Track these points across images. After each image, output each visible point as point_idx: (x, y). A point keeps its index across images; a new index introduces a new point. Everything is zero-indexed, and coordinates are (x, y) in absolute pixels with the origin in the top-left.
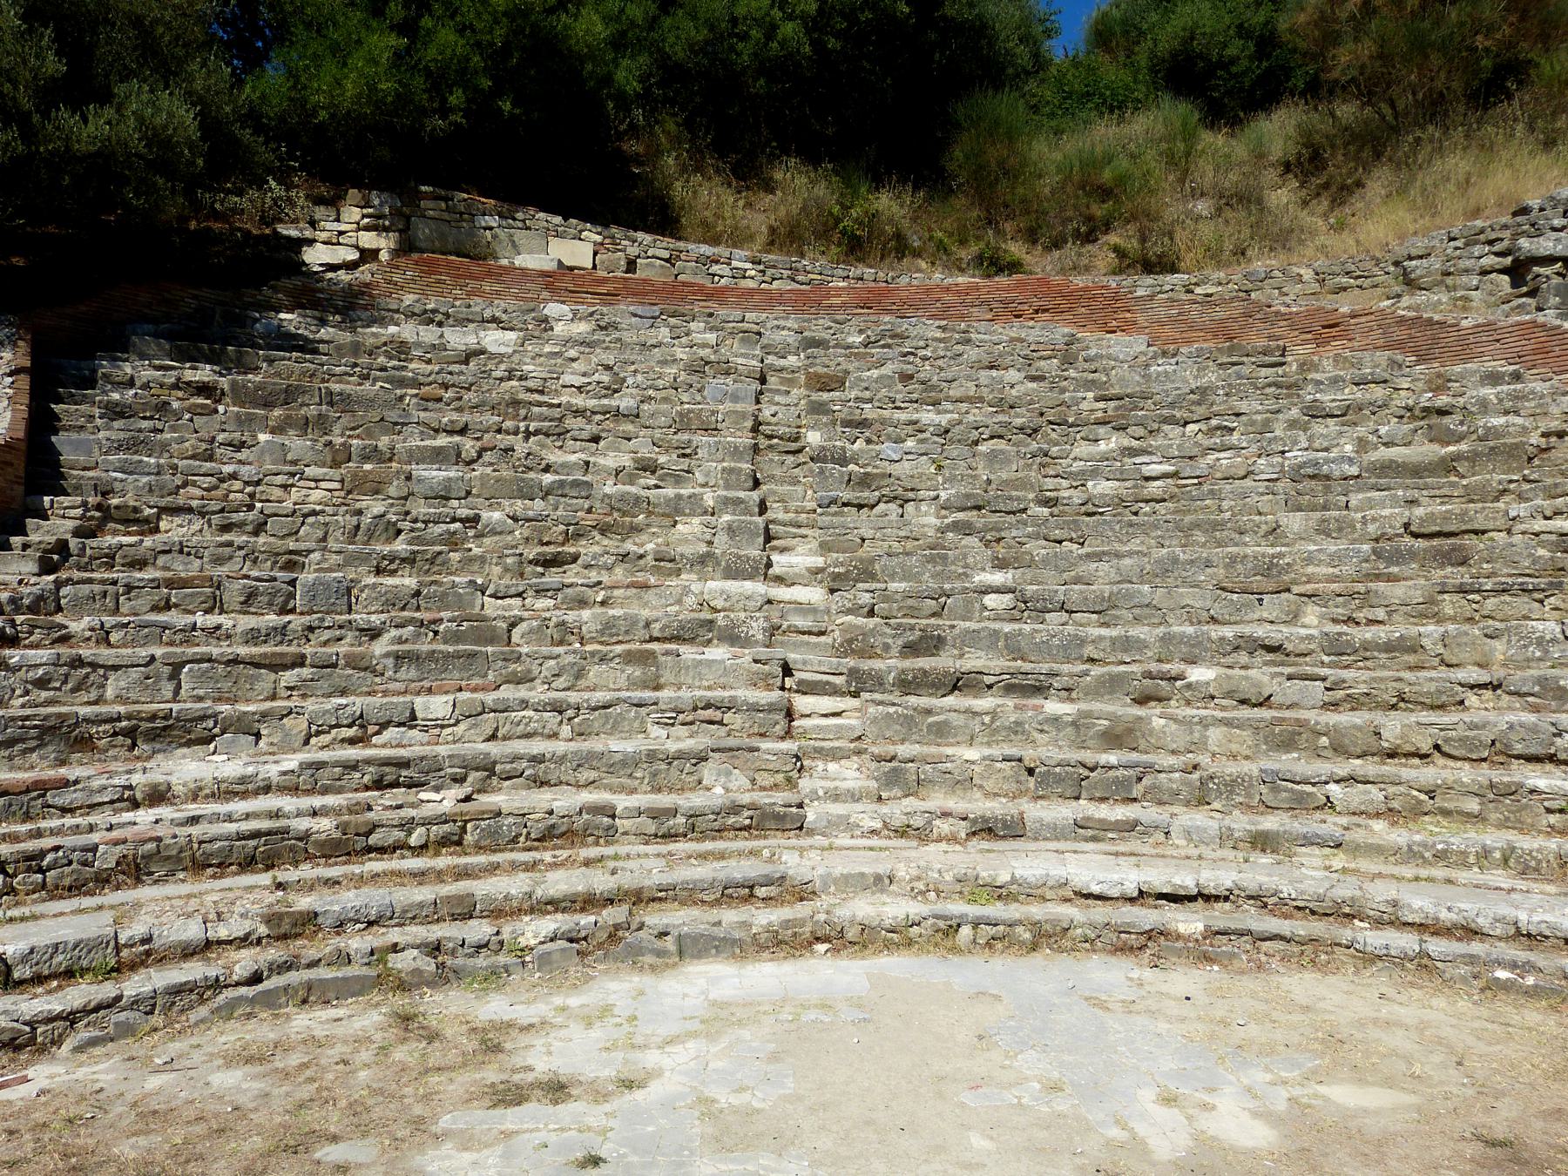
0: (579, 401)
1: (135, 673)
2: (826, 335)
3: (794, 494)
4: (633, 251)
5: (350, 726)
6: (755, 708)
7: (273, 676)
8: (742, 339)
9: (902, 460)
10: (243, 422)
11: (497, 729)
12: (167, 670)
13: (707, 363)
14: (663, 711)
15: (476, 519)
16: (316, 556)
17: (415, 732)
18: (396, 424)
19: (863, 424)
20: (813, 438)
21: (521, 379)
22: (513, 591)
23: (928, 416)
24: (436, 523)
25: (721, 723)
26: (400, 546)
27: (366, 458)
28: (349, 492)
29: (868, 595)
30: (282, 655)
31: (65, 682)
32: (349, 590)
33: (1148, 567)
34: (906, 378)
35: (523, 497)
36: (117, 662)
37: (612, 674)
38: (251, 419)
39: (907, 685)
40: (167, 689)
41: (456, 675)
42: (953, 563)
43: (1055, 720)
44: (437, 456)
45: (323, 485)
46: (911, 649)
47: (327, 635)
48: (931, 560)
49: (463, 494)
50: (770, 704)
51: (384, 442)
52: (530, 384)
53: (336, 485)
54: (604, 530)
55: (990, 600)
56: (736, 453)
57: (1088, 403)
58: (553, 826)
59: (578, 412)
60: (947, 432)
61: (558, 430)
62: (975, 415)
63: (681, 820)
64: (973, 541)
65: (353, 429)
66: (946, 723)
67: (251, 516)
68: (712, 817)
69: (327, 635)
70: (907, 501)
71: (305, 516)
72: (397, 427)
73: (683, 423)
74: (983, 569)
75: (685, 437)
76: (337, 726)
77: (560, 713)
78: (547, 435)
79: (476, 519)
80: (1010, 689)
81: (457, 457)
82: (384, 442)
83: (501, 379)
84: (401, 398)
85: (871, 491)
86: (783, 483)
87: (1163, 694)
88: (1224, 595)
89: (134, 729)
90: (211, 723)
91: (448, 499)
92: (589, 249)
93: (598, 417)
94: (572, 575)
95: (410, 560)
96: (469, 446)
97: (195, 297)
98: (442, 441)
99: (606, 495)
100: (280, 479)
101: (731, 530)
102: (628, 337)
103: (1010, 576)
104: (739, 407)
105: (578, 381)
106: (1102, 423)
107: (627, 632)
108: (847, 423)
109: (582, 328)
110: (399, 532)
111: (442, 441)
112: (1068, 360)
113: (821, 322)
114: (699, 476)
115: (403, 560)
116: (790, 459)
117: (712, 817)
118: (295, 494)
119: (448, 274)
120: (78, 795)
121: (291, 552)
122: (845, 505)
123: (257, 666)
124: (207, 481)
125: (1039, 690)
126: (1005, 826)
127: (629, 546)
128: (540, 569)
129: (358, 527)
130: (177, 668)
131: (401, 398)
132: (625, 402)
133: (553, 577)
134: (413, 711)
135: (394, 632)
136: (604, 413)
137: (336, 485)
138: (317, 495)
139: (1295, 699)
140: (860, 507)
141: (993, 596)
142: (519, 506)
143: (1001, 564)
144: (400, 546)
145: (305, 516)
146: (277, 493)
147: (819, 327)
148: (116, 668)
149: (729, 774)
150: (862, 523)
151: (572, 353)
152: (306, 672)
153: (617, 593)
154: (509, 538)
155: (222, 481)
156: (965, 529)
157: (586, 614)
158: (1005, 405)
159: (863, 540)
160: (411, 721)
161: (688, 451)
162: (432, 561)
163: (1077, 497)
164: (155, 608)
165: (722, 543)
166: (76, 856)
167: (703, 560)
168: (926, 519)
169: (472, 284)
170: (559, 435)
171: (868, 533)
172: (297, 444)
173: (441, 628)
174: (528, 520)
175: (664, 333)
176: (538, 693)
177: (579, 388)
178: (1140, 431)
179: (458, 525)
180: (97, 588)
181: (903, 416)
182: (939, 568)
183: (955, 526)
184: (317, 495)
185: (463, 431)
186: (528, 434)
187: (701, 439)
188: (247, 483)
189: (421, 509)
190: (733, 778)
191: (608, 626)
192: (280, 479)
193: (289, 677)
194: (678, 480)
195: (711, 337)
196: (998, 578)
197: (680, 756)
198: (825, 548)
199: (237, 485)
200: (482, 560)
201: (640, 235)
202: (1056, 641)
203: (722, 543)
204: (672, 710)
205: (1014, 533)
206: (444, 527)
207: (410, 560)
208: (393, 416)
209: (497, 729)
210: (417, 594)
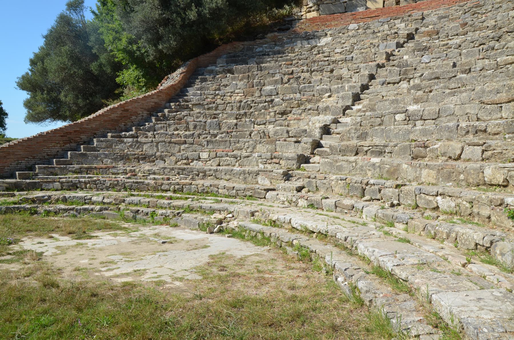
1: (149, 145)
5: (185, 159)
7: (179, 147)
8: (415, 23)
11: (220, 163)
12: (155, 144)
13: (388, 35)
14: (263, 159)
15: (272, 101)
16: (221, 115)
17: (200, 162)
18: (272, 74)
21: (322, 53)
22: (262, 123)
24: (261, 103)
25: (279, 163)
28: (246, 96)
29: (359, 118)
30: (180, 141)
31: (135, 146)
32: (219, 124)
33: (473, 96)
35: (293, 93)
36: (145, 142)
37: (263, 147)
40: (155, 149)
41: (222, 147)
42: (400, 103)
43: (374, 165)
45: (239, 95)
47: (204, 136)
49: (275, 94)
50: (292, 157)
52: (326, 54)
53: (242, 94)
58: (204, 189)
60: (460, 46)
61: (320, 69)
63: (234, 191)
65: (261, 77)
66: (341, 166)
67: (214, 105)
68: (242, 191)
69: (204, 136)
70: (411, 79)
71: (227, 104)
74: (410, 104)
76: (182, 159)
77: (237, 158)
78: (317, 71)
83: (316, 54)
84: (281, 65)
87: (422, 155)
88: (483, 106)
89: (138, 157)
90: (154, 157)
91: (272, 96)
93: (340, 63)
97: (243, 45)
99: (317, 90)
100: (229, 94)
103: (419, 106)
107: (281, 135)
110: (252, 107)
113: (454, 8)
115: (243, 115)
117: (242, 191)
118: (233, 98)
119: (319, 22)
120: (116, 170)
121: (215, 114)
122: (389, 83)
123: (175, 144)
124: (211, 97)
126: (317, 204)
128: (280, 116)
129: (240, 106)
130: (157, 143)
131: (281, 65)
134: (199, 156)
135: (220, 135)
136: (342, 61)
137: (242, 94)
139: (470, 157)
140: (394, 83)
141: (398, 115)
145: (227, 104)
146: (229, 98)
148: (145, 143)
149: (264, 179)
152: (186, 146)
153: (291, 122)
154: (281, 107)
155: (215, 96)
159: (383, 97)
160: (199, 159)
161: (358, 70)
162: (250, 115)
164: (174, 130)
166: (102, 182)
169: (328, 23)
170: (321, 70)
173: (232, 134)
174: (286, 100)
177: (340, 53)
179: (266, 103)
180: (162, 125)
182: (395, 105)
188: (221, 96)
190: (265, 181)
192: (229, 94)
193: (183, 147)
199: (219, 97)
202: (401, 132)
204: (265, 158)
205: (436, 87)
206: (262, 104)
209: (220, 163)
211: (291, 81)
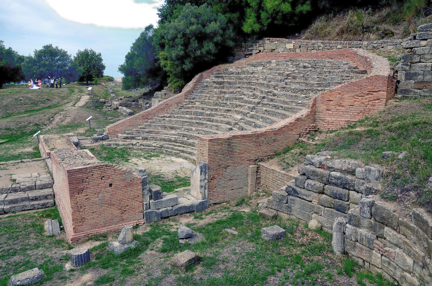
4: (300, 44)
92: (292, 45)
211: (237, 93)
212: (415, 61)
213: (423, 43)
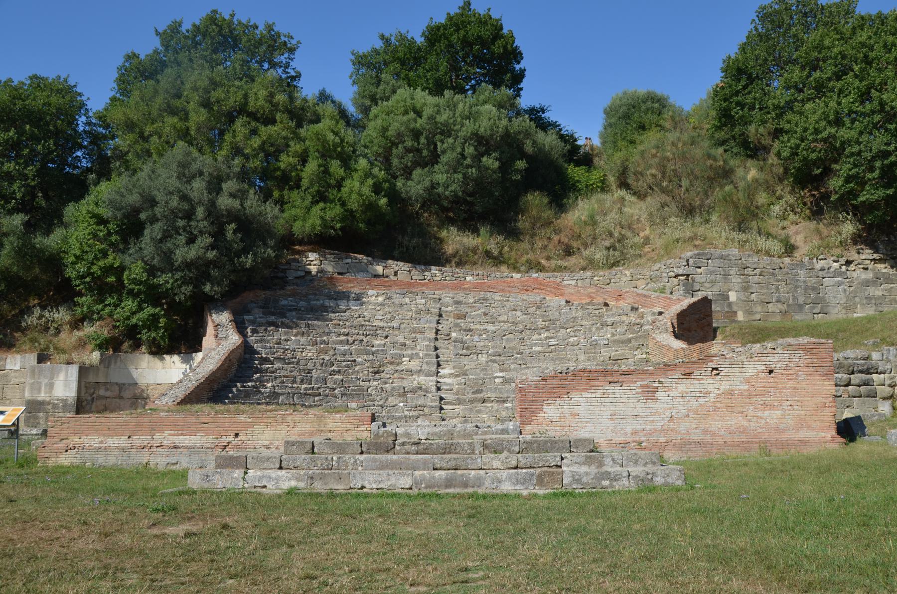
0: (381, 324)
2: (462, 299)
3: (447, 352)
4: (397, 268)
6: (432, 407)
9: (477, 341)
10: (286, 333)
19: (470, 330)
20: (454, 335)
23: (490, 327)
26: (335, 368)
27: (321, 344)
34: (485, 314)
38: (288, 332)
39: (471, 401)
43: (507, 408)
44: (341, 342)
46: (474, 393)
48: (482, 370)
51: (325, 338)
54: (391, 363)
55: (497, 380)
56: (429, 340)
57: (540, 323)
59: (381, 328)
62: (505, 326)
64: (495, 365)
72: (328, 334)
73: (414, 330)
75: (413, 335)
79: (355, 361)
80: (497, 401)
81: (347, 342)
82: (325, 338)
85: (469, 350)
86: (172, 493)
94: (382, 375)
95: (339, 371)
96: (351, 340)
98: (343, 338)
101: (427, 363)
102: (396, 301)
104: (431, 325)
105: (380, 318)
106: (542, 329)
108: (465, 330)
109: (381, 299)
111: (343, 338)
112: (538, 308)
114: (418, 348)
116: (446, 342)
125: (505, 401)
127: (398, 368)
130: (294, 395)
132: (395, 324)
133: (377, 376)
138: (310, 354)
142: (365, 357)
143: (502, 371)
144: (335, 368)
147: (460, 297)
150: (465, 361)
151: (378, 308)
156: (494, 361)
157: (387, 385)
158: (514, 323)
163: (528, 351)
165: (425, 367)
167: (419, 371)
168: (483, 358)
171: (466, 363)
172: (303, 340)
175: (407, 300)
176: (376, 403)
178: (553, 331)
181: (482, 327)
183: (491, 361)
184: (310, 354)
185: (347, 335)
186: (367, 335)
187: (419, 336)
189: (339, 358)
191: (393, 389)
193: (316, 399)
194: (412, 349)
195: (423, 301)
196: (501, 374)
197: (413, 416)
198: (454, 367)
200: (358, 372)
201: (399, 263)
203: (425, 367)
207: (339, 371)
208: (327, 331)
210: (342, 380)
212: (695, 289)
213: (699, 270)
